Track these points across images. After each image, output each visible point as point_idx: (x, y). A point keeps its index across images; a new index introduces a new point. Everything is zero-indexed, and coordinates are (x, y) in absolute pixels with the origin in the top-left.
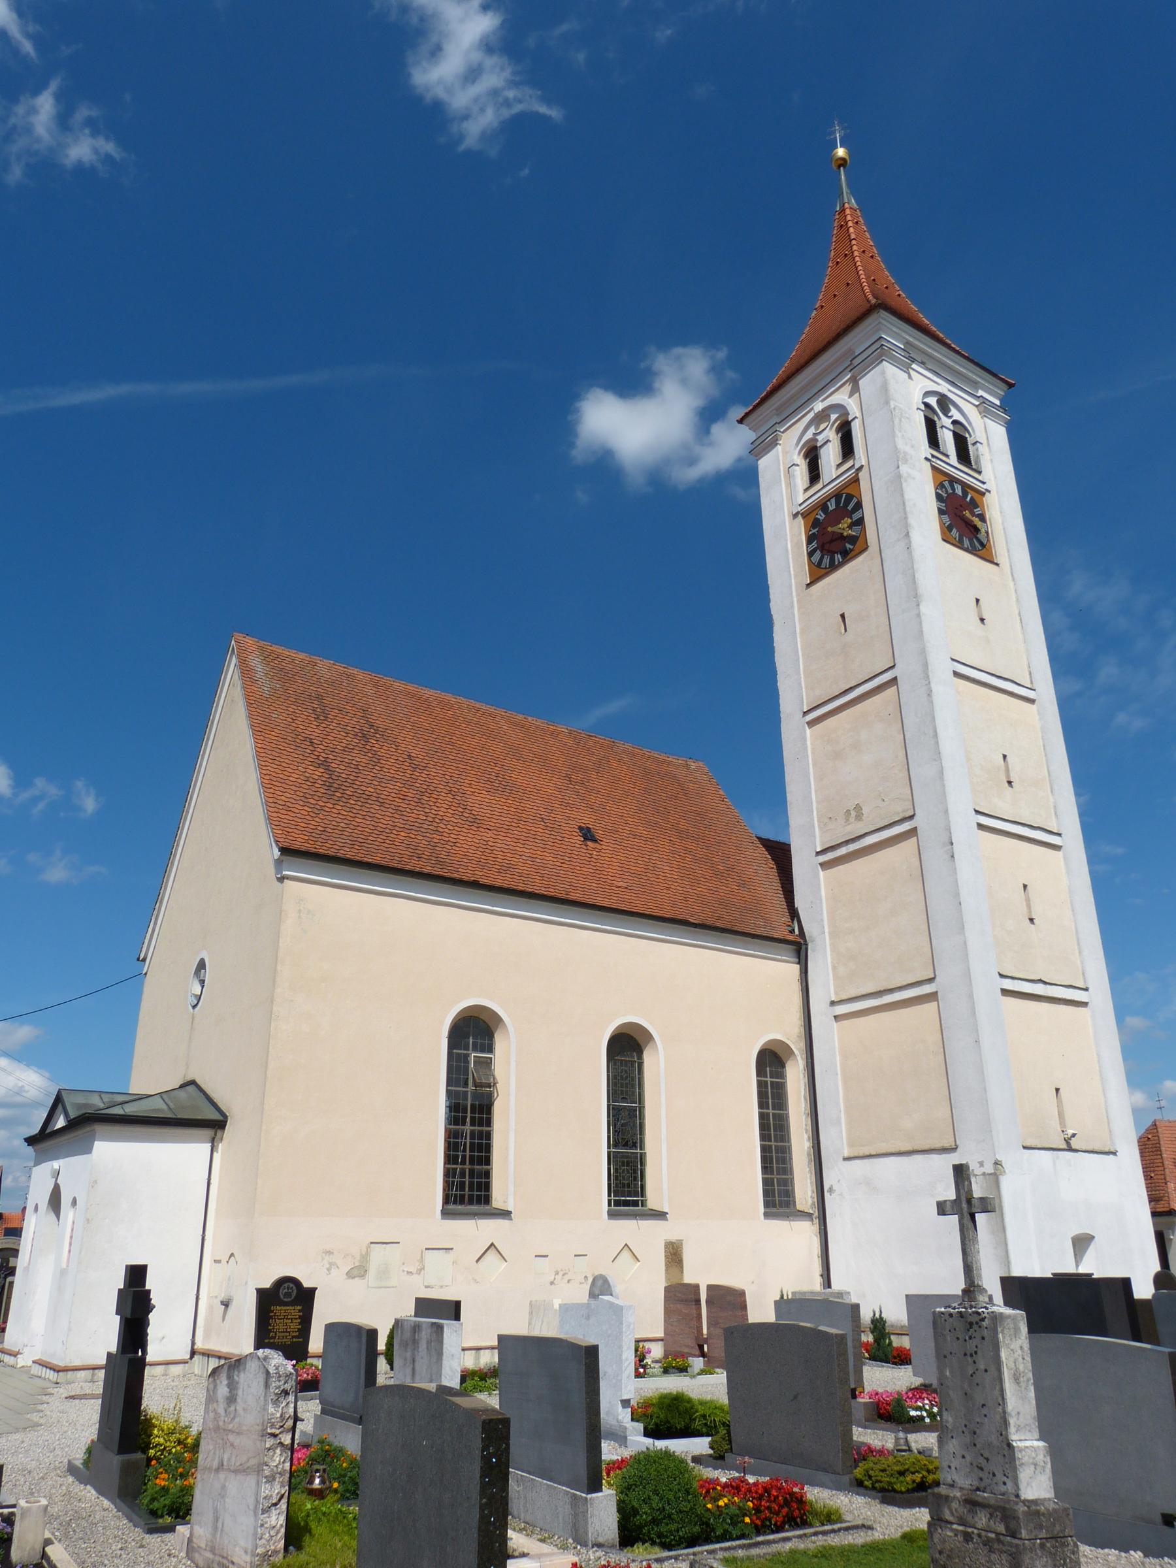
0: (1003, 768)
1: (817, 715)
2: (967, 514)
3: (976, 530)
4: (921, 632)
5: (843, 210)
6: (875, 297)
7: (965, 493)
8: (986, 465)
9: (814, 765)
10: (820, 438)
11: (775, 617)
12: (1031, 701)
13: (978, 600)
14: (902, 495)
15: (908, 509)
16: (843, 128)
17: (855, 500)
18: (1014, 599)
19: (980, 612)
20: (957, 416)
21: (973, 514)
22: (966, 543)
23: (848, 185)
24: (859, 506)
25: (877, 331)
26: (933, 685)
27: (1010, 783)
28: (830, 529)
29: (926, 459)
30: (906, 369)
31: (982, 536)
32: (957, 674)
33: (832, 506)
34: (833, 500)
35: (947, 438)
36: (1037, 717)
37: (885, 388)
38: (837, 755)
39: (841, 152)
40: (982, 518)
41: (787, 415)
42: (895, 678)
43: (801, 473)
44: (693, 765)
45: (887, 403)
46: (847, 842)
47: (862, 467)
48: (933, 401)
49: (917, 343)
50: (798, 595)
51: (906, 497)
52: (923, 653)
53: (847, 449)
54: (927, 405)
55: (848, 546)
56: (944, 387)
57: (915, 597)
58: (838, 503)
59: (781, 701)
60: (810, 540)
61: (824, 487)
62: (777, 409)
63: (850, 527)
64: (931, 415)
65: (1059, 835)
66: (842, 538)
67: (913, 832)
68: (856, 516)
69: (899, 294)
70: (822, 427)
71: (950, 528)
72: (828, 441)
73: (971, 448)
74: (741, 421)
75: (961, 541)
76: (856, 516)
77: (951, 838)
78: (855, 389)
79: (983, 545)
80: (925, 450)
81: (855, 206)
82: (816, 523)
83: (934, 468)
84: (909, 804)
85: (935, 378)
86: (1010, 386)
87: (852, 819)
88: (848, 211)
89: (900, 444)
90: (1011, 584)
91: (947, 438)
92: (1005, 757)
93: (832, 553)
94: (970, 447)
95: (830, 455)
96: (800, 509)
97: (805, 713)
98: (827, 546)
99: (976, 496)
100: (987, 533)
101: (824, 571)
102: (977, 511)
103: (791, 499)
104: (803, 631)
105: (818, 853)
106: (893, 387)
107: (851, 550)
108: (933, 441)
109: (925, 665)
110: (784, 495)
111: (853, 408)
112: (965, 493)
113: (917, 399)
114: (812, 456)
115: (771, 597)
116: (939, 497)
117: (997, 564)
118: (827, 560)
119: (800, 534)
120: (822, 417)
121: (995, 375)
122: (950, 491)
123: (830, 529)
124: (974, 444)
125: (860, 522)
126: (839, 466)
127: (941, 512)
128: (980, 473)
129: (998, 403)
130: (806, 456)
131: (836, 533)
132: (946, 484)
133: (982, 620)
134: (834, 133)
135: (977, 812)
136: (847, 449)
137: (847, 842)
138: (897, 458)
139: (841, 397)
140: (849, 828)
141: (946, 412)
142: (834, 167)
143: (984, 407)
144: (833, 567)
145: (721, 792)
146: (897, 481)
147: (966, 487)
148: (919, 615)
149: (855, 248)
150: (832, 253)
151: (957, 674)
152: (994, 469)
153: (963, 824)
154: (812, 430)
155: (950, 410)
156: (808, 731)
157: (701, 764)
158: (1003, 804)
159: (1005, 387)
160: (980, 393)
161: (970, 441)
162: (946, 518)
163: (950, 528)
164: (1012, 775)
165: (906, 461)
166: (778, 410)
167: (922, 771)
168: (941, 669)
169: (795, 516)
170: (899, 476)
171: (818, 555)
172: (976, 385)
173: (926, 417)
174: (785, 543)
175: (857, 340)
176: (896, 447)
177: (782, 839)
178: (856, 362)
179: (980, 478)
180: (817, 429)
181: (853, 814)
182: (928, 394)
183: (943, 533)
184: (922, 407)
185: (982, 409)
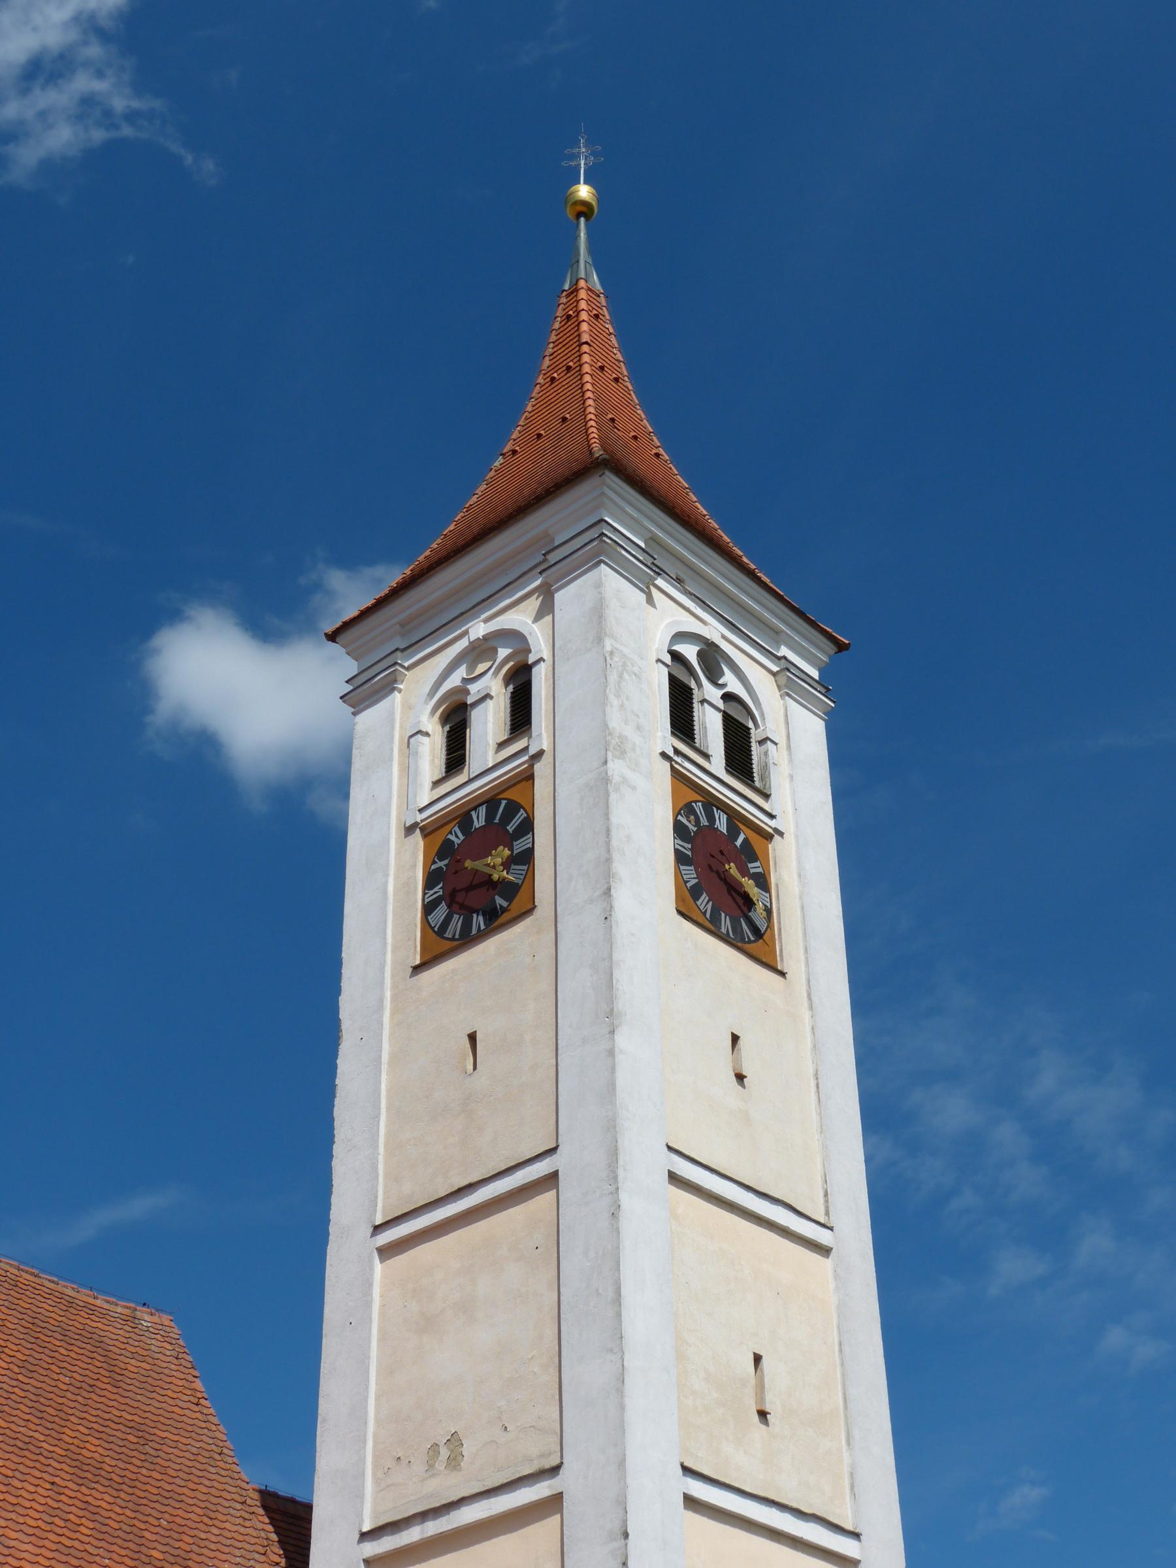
0: (753, 1381)
1: (403, 1234)
2: (733, 869)
3: (748, 902)
4: (612, 1086)
5: (575, 290)
7: (733, 831)
8: (780, 784)
9: (382, 1339)
10: (474, 688)
11: (346, 1025)
12: (823, 1250)
13: (735, 1039)
14: (607, 816)
15: (614, 843)
16: (593, 154)
19: (737, 1061)
20: (733, 684)
21: (744, 872)
22: (726, 924)
23: (591, 250)
24: (527, 826)
26: (624, 1198)
27: (763, 1414)
28: (468, 864)
29: (664, 755)
30: (646, 587)
31: (758, 915)
32: (674, 1179)
33: (479, 820)
34: (483, 810)
35: (710, 725)
36: (832, 1285)
37: (598, 614)
38: (428, 1324)
39: (584, 191)
40: (762, 881)
41: (420, 636)
42: (554, 1176)
44: (146, 1319)
45: (599, 640)
46: (424, 1516)
47: (540, 754)
48: (690, 652)
49: (670, 541)
51: (614, 820)
52: (611, 1128)
53: (520, 716)
54: (676, 657)
55: (500, 901)
56: (714, 631)
57: (609, 1017)
58: (490, 816)
59: (335, 1199)
60: (431, 880)
61: (471, 781)
62: (403, 625)
63: (506, 865)
64: (682, 676)
65: (856, 1535)
66: (489, 884)
67: (554, 1503)
68: (520, 846)
69: (655, 454)
70: (481, 668)
71: (695, 892)
72: (487, 696)
74: (332, 637)
75: (715, 919)
76: (520, 846)
77: (625, 1521)
78: (547, 608)
79: (758, 934)
80: (663, 737)
81: (598, 287)
82: (446, 850)
83: (676, 774)
84: (553, 1442)
86: (841, 647)
87: (440, 1465)
88: (583, 294)
89: (615, 721)
90: (806, 1015)
91: (710, 725)
92: (757, 1359)
93: (468, 911)
94: (754, 747)
95: (488, 724)
96: (419, 817)
97: (377, 1229)
98: (460, 897)
99: (754, 839)
100: (769, 911)
101: (448, 945)
104: (395, 1059)
105: (364, 1536)
106: (613, 612)
107: (504, 910)
108: (682, 721)
109: (614, 1153)
110: (394, 788)
111: (540, 645)
112: (733, 831)
113: (659, 644)
114: (456, 720)
115: (344, 984)
116: (680, 830)
117: (782, 974)
118: (457, 923)
119: (414, 866)
120: (482, 650)
121: (813, 624)
122: (704, 822)
123: (468, 864)
124: (761, 742)
125: (527, 857)
127: (680, 858)
128: (766, 796)
129: (815, 674)
130: (445, 719)
131: (480, 874)
132: (698, 807)
133: (740, 1077)
135: (687, 1470)
136: (520, 716)
137: (424, 1516)
138: (607, 745)
139: (520, 618)
140: (433, 1484)
141: (714, 677)
142: (570, 214)
144: (467, 939)
145: (198, 1384)
147: (735, 817)
148: (611, 1053)
149: (586, 358)
150: (547, 362)
151: (674, 1179)
152: (793, 793)
153: (654, 1493)
154: (461, 672)
156: (378, 1267)
157: (166, 1319)
158: (745, 1459)
159: (831, 649)
160: (784, 651)
162: (690, 873)
163: (695, 892)
164: (769, 1397)
165: (623, 754)
167: (586, 1373)
168: (644, 1165)
169: (410, 830)
170: (605, 780)
171: (441, 911)
172: (776, 636)
174: (383, 883)
175: (557, 519)
176: (605, 725)
177: (300, 1496)
179: (766, 806)
180: (471, 669)
181: (444, 1453)
182: (681, 636)
183: (679, 899)
184: (668, 659)
185: (782, 680)
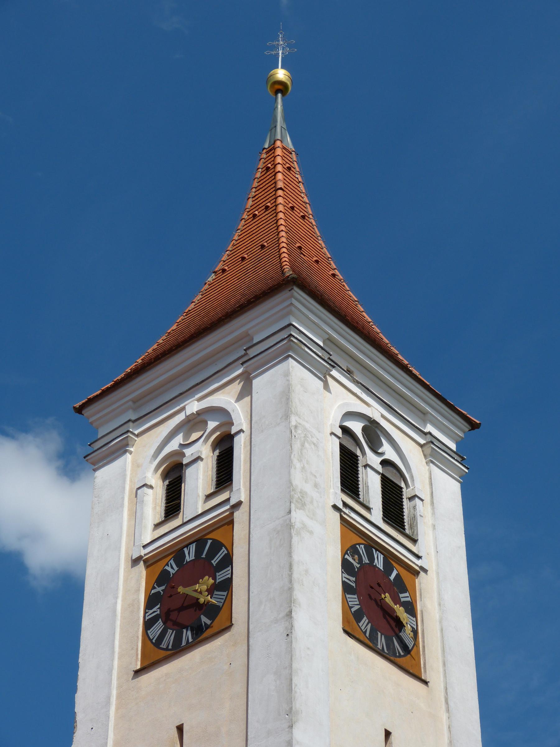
2: (388, 599)
5: (273, 149)
6: (292, 268)
11: (80, 717)
14: (290, 554)
15: (295, 575)
16: (289, 46)
17: (223, 552)
18: (446, 741)
20: (390, 453)
21: (397, 600)
22: (381, 642)
24: (228, 561)
25: (289, 313)
28: (181, 589)
29: (335, 507)
33: (190, 555)
34: (193, 547)
35: (371, 484)
37: (286, 396)
40: (411, 608)
41: (148, 410)
43: (154, 500)
45: (287, 417)
47: (239, 504)
48: (357, 427)
50: (119, 686)
51: (295, 557)
53: (224, 475)
54: (346, 431)
56: (375, 411)
57: (289, 715)
58: (198, 552)
62: (134, 401)
63: (210, 591)
68: (221, 576)
70: (194, 436)
71: (358, 616)
72: (199, 458)
73: (406, 503)
75: (373, 638)
76: (221, 576)
78: (246, 391)
79: (407, 650)
80: (335, 493)
81: (291, 146)
82: (163, 578)
85: (364, 396)
86: (474, 426)
88: (279, 152)
89: (297, 479)
90: (444, 716)
91: (371, 484)
93: (179, 627)
94: (405, 502)
95: (199, 480)
96: (143, 552)
98: (174, 616)
99: (405, 574)
100: (415, 632)
101: (163, 654)
102: (404, 597)
103: (134, 534)
106: (299, 397)
107: (208, 627)
108: (350, 482)
112: (388, 568)
113: (333, 421)
114: (174, 476)
115: (80, 684)
116: (346, 566)
117: (426, 683)
118: (170, 636)
119: (138, 590)
120: (195, 422)
121: (452, 407)
122: (366, 560)
123: (181, 589)
124: (411, 499)
125: (226, 585)
126: (209, 497)
127: (347, 589)
128: (414, 541)
129: (453, 446)
130: (165, 475)
131: (189, 597)
132: (361, 549)
134: (276, 48)
136: (224, 475)
138: (290, 498)
139: (225, 398)
141: (375, 447)
143: (432, 449)
144: (178, 649)
146: (286, 531)
147: (389, 557)
149: (280, 200)
150: (250, 202)
152: (435, 539)
155: (381, 445)
159: (466, 427)
160: (429, 428)
161: (406, 493)
162: (354, 600)
163: (358, 616)
165: (302, 505)
166: (137, 402)
170: (289, 526)
172: (423, 415)
173: (343, 448)
175: (257, 323)
176: (290, 482)
178: (252, 352)
180: (186, 437)
182: (349, 415)
183: (345, 620)
184: (339, 432)
185: (428, 450)
